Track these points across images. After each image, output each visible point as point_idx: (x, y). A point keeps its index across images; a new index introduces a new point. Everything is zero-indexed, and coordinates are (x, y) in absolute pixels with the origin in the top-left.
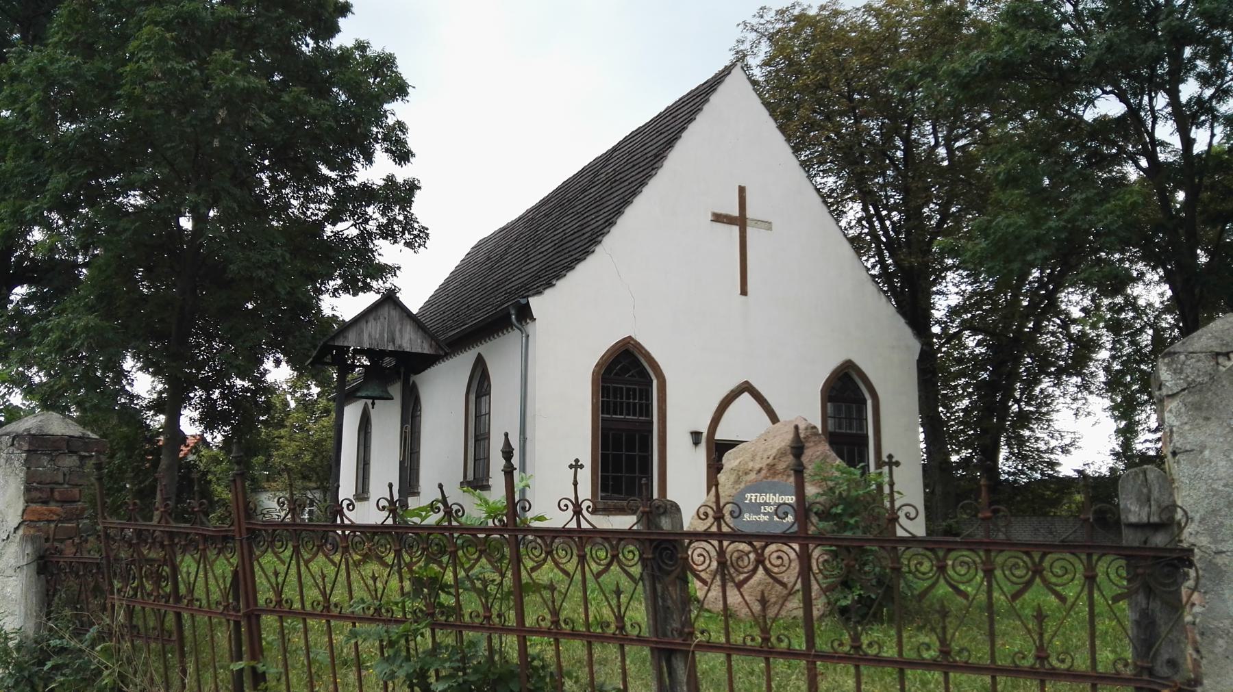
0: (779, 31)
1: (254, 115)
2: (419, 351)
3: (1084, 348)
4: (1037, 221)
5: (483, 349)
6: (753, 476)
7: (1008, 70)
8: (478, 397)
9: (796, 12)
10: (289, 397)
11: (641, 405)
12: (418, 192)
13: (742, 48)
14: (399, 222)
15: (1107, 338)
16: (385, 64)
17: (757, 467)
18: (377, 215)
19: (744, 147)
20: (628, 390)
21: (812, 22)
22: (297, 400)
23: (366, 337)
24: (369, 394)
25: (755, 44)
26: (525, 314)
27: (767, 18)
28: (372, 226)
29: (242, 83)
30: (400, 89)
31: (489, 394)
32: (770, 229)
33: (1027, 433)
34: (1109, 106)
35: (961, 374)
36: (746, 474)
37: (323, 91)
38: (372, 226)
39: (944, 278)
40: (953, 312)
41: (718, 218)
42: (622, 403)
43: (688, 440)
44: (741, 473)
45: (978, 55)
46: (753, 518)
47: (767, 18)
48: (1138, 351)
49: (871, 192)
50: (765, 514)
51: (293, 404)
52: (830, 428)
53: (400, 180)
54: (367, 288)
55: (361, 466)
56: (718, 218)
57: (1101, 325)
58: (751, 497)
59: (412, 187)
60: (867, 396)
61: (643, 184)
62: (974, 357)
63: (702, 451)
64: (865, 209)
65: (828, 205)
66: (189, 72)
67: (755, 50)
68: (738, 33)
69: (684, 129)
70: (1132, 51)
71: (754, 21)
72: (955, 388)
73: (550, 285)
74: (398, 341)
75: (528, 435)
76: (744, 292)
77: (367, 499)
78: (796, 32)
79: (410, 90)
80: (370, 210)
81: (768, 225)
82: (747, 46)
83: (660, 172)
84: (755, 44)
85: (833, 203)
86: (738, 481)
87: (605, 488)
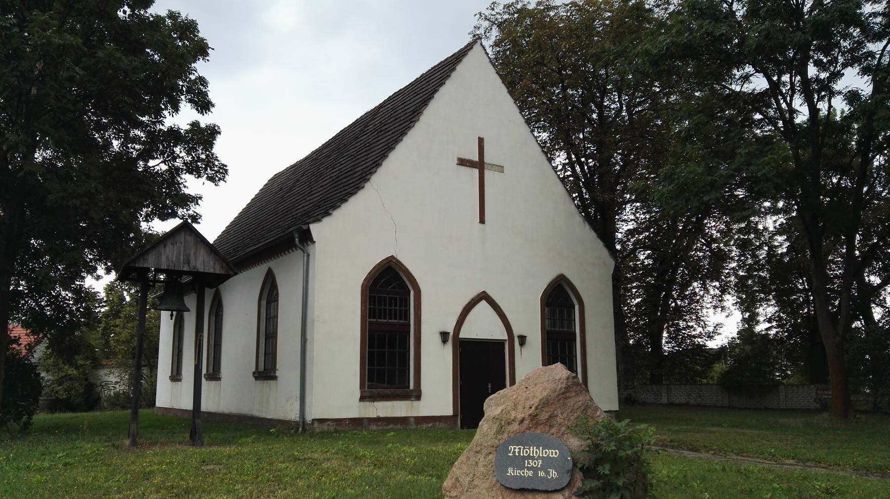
0: (506, 20)
1: (68, 68)
2: (212, 271)
3: (720, 258)
4: (710, 171)
5: (271, 264)
6: (515, 427)
7: (688, 51)
8: (268, 303)
9: (519, 7)
10: (125, 293)
11: (401, 311)
12: (219, 138)
13: (478, 32)
14: (203, 160)
15: (735, 252)
16: (188, 28)
17: (520, 416)
18: (183, 154)
19: (482, 107)
20: (391, 299)
21: (531, 14)
22: (131, 295)
23: (164, 259)
24: (167, 307)
25: (488, 30)
26: (307, 238)
27: (496, 10)
28: (179, 163)
29: (57, 40)
30: (201, 50)
31: (277, 301)
32: (502, 172)
33: (682, 324)
34: (759, 83)
35: (636, 279)
36: (509, 424)
37: (136, 49)
38: (179, 163)
39: (625, 209)
40: (630, 233)
41: (462, 162)
42: (385, 310)
43: (438, 339)
44: (503, 423)
45: (664, 40)
46: (518, 472)
47: (496, 10)
48: (757, 262)
49: (573, 145)
50: (529, 469)
51: (128, 299)
52: (547, 328)
53: (203, 125)
54: (174, 215)
55: (176, 353)
56: (462, 162)
57: (732, 243)
58: (514, 449)
59: (212, 132)
60: (575, 302)
61: (403, 133)
62: (645, 267)
63: (449, 347)
64: (569, 157)
65: (546, 153)
66: (9, 29)
67: (488, 35)
68: (475, 21)
69: (436, 91)
70: (784, 38)
71: (487, 13)
72: (630, 290)
73: (327, 214)
74: (193, 263)
75: (308, 337)
76: (482, 221)
77: (180, 380)
78: (518, 22)
79: (210, 51)
80: (177, 150)
81: (501, 169)
82: (482, 31)
83: (417, 125)
84: (488, 30)
85: (548, 153)
86: (500, 431)
87: (370, 379)
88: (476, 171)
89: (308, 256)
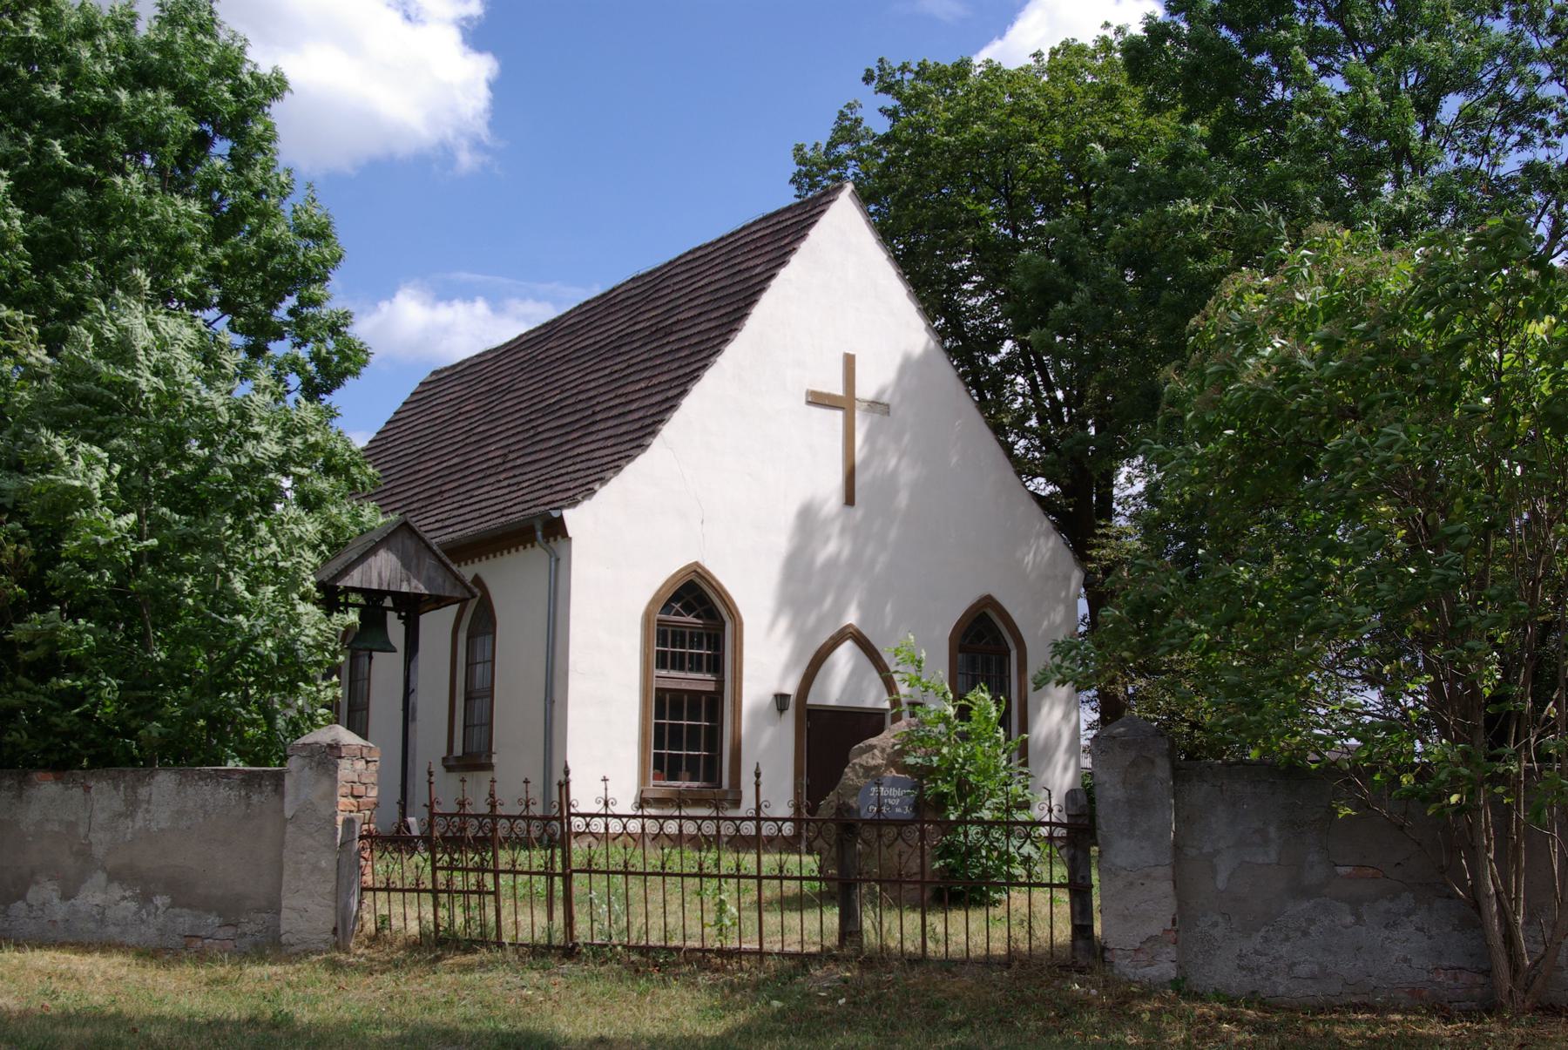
8: (471, 637)
41: (818, 400)
56: (818, 400)
60: (1012, 645)
63: (790, 713)
88: (838, 416)
89: (558, 560)
